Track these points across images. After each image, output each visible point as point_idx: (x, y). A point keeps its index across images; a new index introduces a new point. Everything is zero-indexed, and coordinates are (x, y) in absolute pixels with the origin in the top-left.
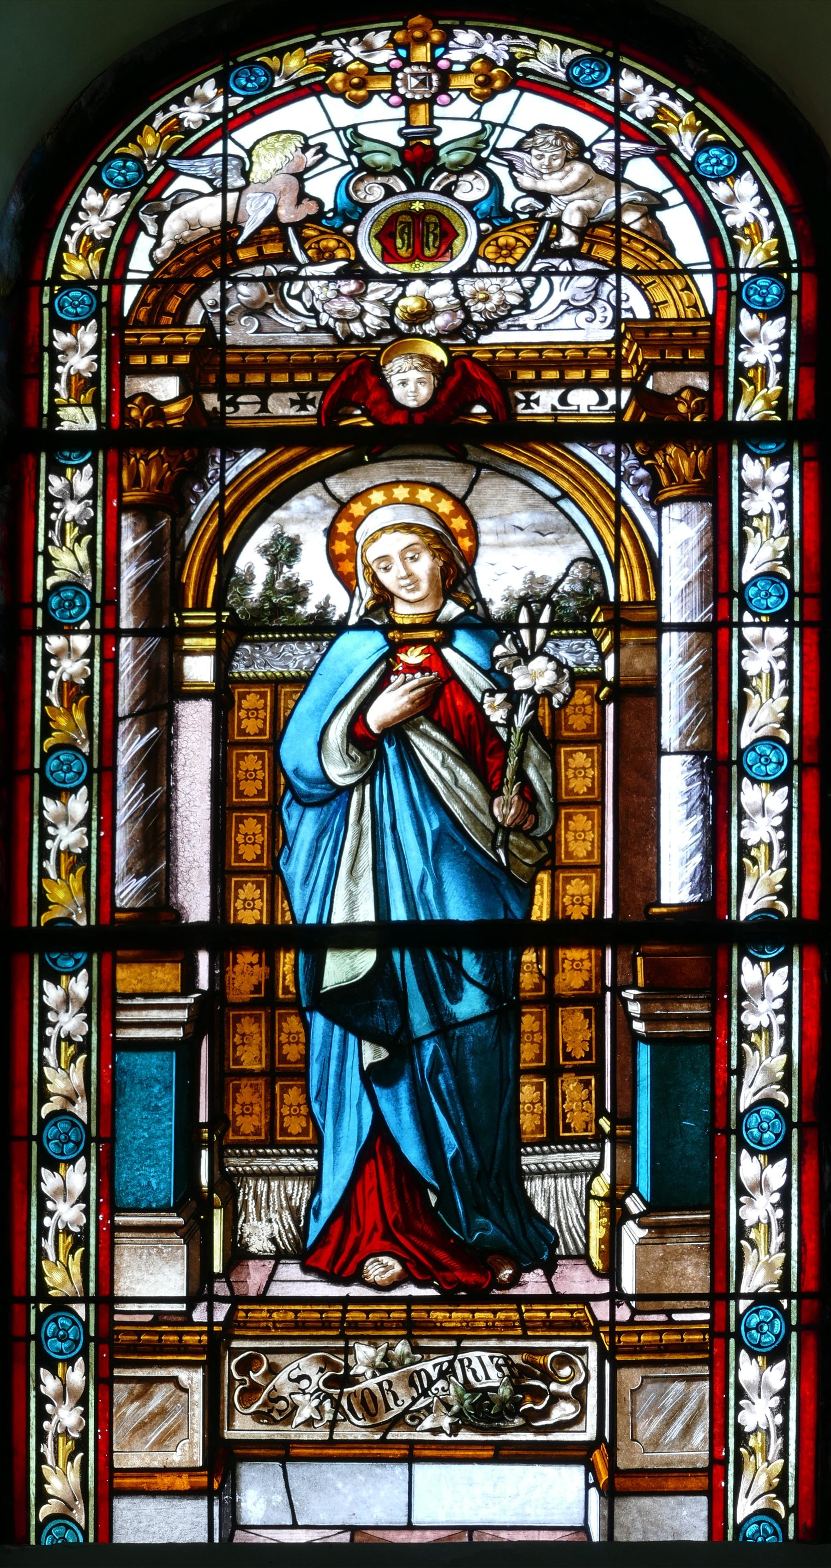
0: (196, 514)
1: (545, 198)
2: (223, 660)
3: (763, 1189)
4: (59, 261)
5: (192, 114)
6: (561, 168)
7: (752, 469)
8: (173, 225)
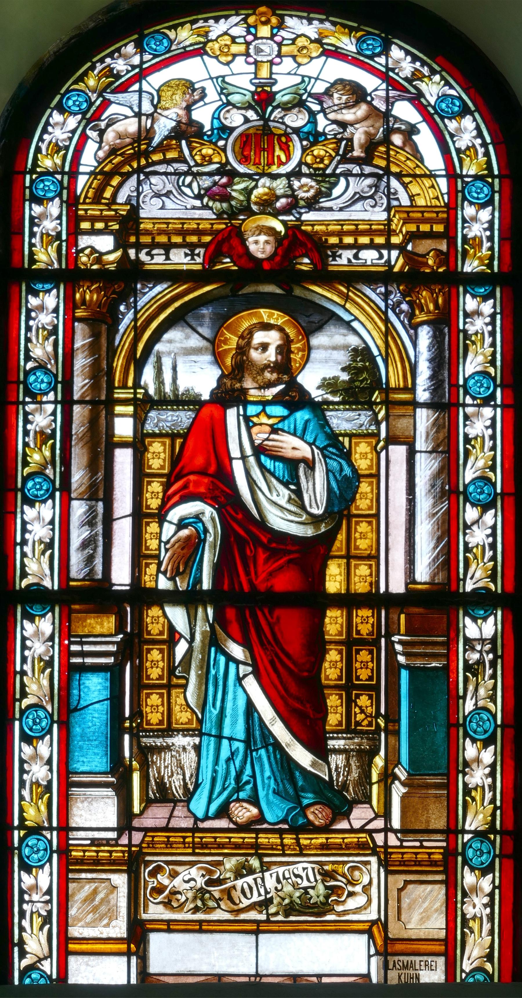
0: (122, 328)
1: (343, 125)
2: (139, 420)
3: (481, 762)
4: (35, 159)
5: (120, 65)
6: (353, 106)
7: (471, 304)
8: (110, 136)
